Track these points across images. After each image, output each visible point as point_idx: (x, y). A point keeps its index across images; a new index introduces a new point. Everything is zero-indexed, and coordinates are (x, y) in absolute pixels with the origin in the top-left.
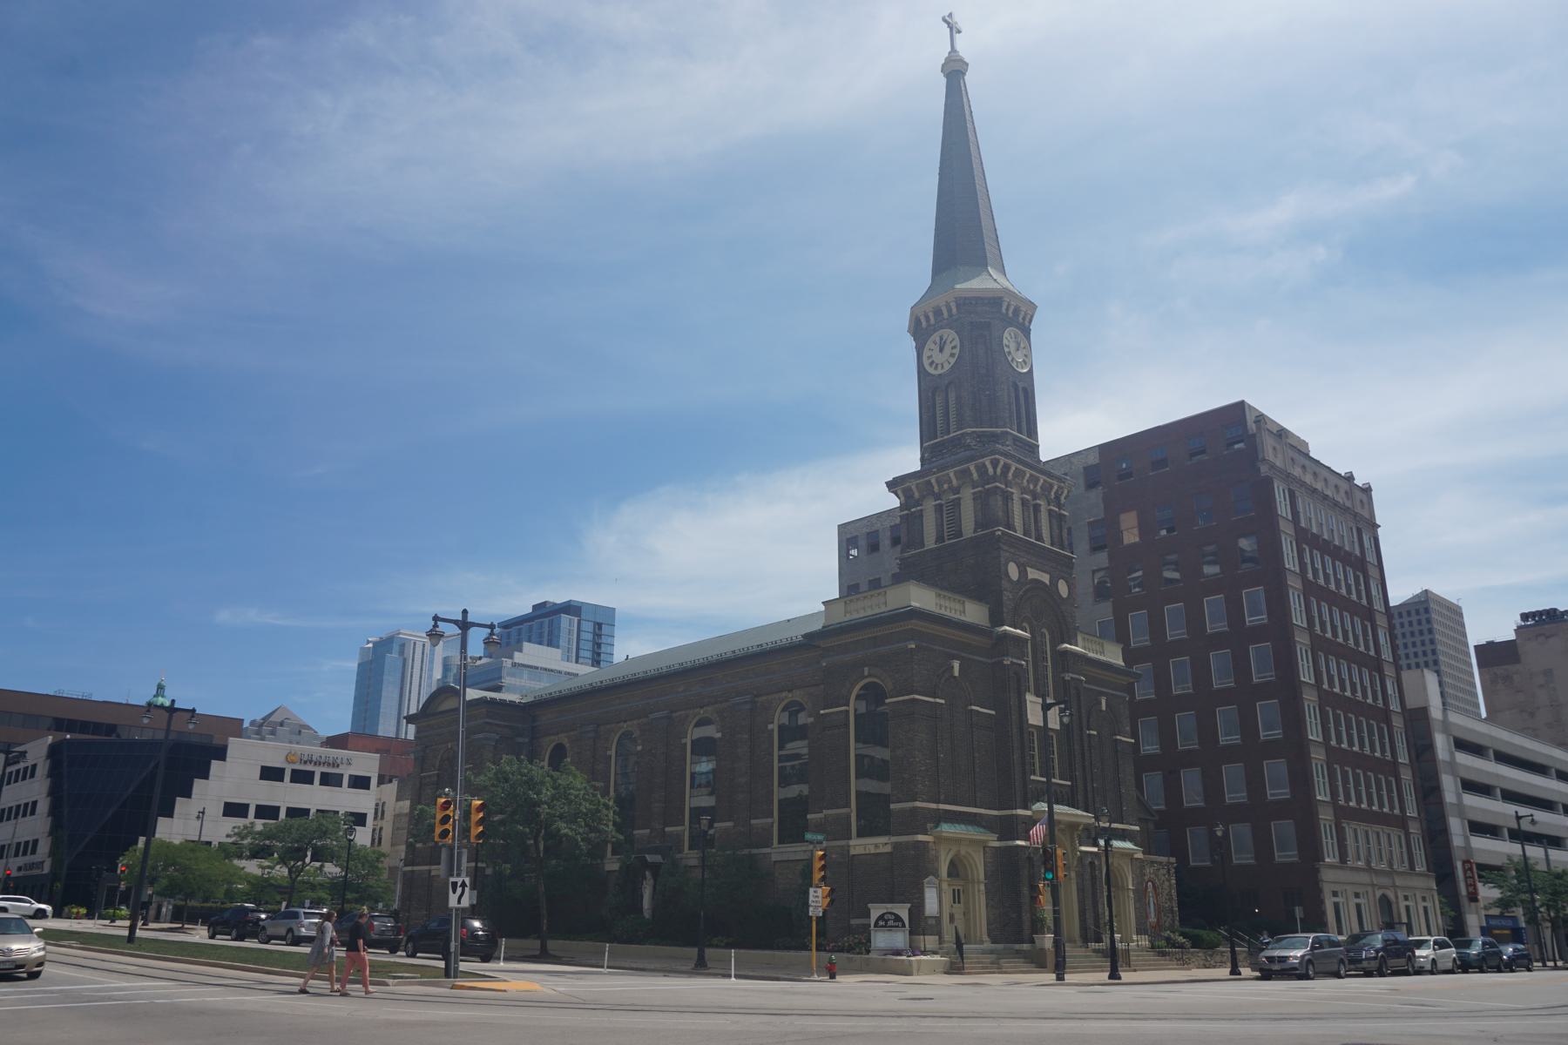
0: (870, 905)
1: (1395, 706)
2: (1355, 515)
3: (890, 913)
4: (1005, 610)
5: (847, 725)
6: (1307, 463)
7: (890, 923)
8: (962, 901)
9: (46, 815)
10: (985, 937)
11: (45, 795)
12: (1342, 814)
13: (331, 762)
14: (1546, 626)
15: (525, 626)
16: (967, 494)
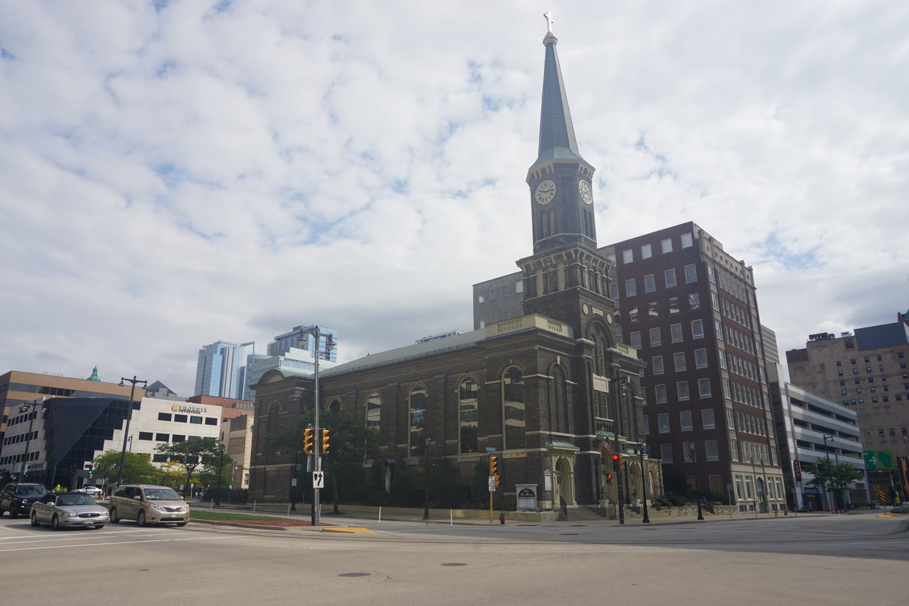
0: (516, 485)
1: (763, 382)
2: (745, 283)
3: (527, 489)
4: (582, 330)
5: (500, 390)
6: (723, 255)
7: (527, 494)
9: (43, 439)
11: (42, 428)
12: (741, 437)
13: (196, 411)
14: (822, 342)
15: (289, 340)
16: (561, 268)
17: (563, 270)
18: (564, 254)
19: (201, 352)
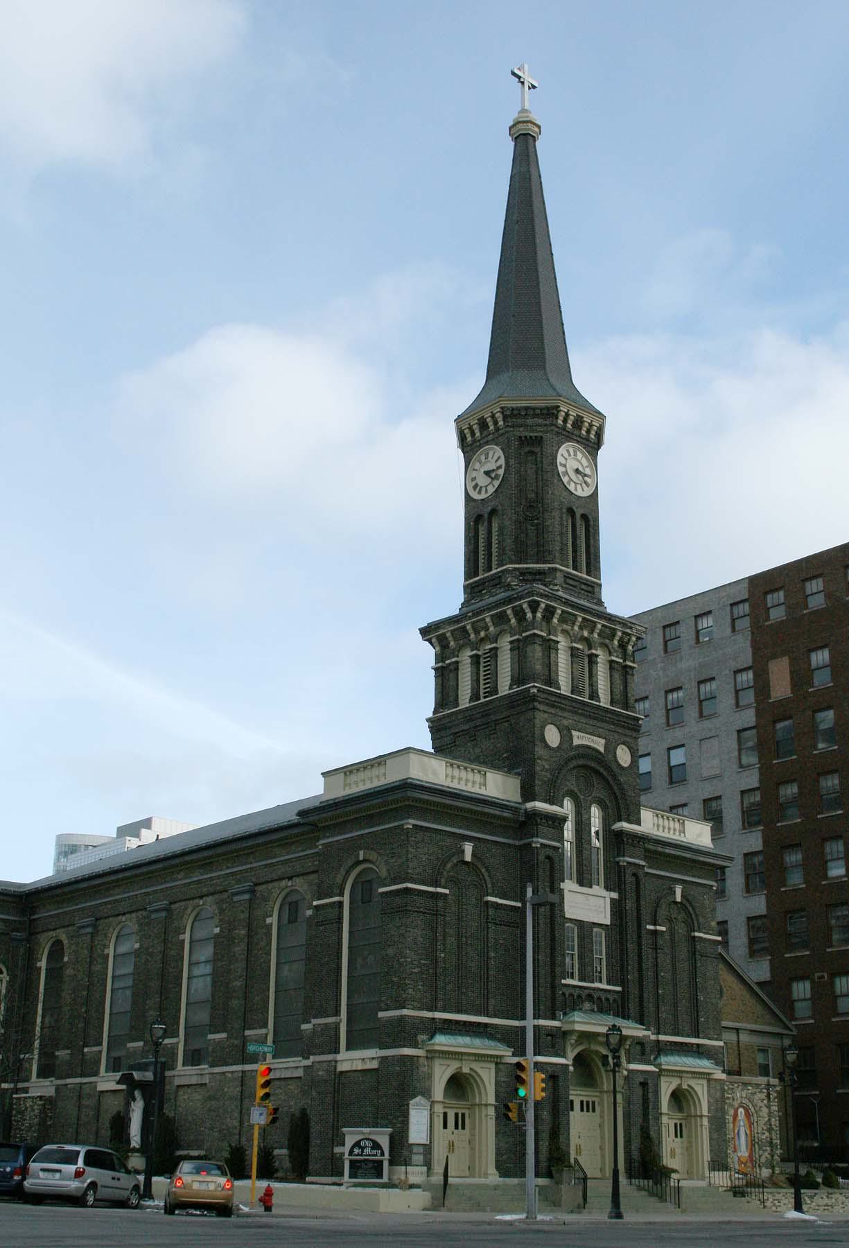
0: (345, 1130)
8: (467, 1127)
10: (492, 1170)
17: (509, 647)
18: (509, 612)
19: (57, 836)
